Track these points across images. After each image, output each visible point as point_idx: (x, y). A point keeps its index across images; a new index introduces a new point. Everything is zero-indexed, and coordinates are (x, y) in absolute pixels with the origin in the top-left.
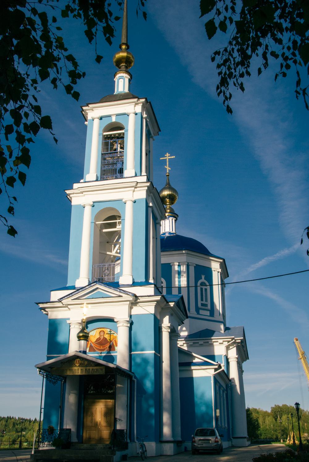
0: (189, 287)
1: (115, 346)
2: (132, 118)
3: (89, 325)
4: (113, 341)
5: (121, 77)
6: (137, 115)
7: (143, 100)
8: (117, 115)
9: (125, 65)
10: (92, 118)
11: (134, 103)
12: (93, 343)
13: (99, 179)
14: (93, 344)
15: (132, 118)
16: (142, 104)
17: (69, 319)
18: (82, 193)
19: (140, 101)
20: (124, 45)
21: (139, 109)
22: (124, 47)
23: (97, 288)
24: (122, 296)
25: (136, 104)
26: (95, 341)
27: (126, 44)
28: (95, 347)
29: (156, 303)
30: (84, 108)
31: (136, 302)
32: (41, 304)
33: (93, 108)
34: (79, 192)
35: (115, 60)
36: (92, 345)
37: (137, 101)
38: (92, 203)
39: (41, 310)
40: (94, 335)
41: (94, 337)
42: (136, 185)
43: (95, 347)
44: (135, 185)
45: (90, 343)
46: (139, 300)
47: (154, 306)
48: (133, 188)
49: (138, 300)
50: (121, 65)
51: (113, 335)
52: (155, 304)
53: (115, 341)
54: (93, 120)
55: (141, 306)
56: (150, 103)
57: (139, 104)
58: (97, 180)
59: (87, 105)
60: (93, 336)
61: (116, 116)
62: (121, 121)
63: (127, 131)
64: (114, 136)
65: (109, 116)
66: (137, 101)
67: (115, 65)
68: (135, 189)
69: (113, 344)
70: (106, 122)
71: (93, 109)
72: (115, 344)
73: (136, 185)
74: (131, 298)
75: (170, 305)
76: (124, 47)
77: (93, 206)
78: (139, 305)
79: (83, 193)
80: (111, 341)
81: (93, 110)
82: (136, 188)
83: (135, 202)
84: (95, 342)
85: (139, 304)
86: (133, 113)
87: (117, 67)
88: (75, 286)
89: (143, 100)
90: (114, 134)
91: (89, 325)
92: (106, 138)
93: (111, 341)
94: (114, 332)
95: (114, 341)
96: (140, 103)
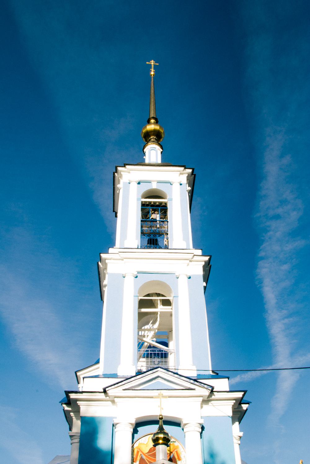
0: (213, 391)
1: (177, 460)
2: (176, 187)
3: (139, 429)
4: (173, 453)
5: (154, 149)
6: (181, 186)
7: (190, 171)
8: (159, 182)
9: (155, 138)
10: (129, 181)
11: (179, 173)
12: (144, 455)
13: (139, 247)
14: (146, 456)
15: (176, 187)
16: (187, 175)
17: (116, 418)
18: (122, 260)
19: (186, 170)
20: (154, 119)
21: (184, 179)
22: (152, 121)
23: (158, 377)
24: (194, 389)
25: (181, 174)
26: (147, 452)
27: (156, 119)
28: (147, 460)
29: (234, 401)
30: (119, 169)
31: (208, 399)
32: (74, 394)
33: (130, 170)
34: (119, 257)
35: (144, 131)
36: (144, 457)
37: (183, 171)
38: (137, 273)
39: (62, 405)
40: (145, 443)
41: (147, 446)
42: (192, 258)
43: (147, 460)
44: (191, 257)
45: (141, 455)
46: (215, 396)
47: (232, 406)
48: (188, 261)
49: (213, 397)
50: (151, 137)
51: (173, 444)
52: (233, 404)
53: (177, 452)
54: (129, 183)
55: (213, 406)
56: (195, 175)
57: (184, 175)
58: (138, 248)
59: (124, 166)
60: (144, 444)
61: (157, 182)
62: (162, 188)
63: (171, 200)
64: (154, 203)
65: (149, 182)
66: (183, 171)
67: (142, 136)
68: (190, 263)
69: (174, 457)
70: (145, 188)
71: (131, 171)
72: (176, 457)
73: (192, 258)
74: (207, 393)
75: (242, 407)
76: (152, 121)
77: (136, 277)
78: (212, 404)
79: (124, 259)
80: (172, 453)
81: (129, 173)
82: (190, 261)
83: (190, 278)
84: (148, 453)
85: (211, 402)
86: (179, 183)
87: (144, 139)
88: (117, 374)
89: (190, 171)
90: (148, 202)
91: (139, 429)
92: (144, 205)
93: (172, 453)
94: (174, 440)
95: (175, 453)
96: (184, 174)
